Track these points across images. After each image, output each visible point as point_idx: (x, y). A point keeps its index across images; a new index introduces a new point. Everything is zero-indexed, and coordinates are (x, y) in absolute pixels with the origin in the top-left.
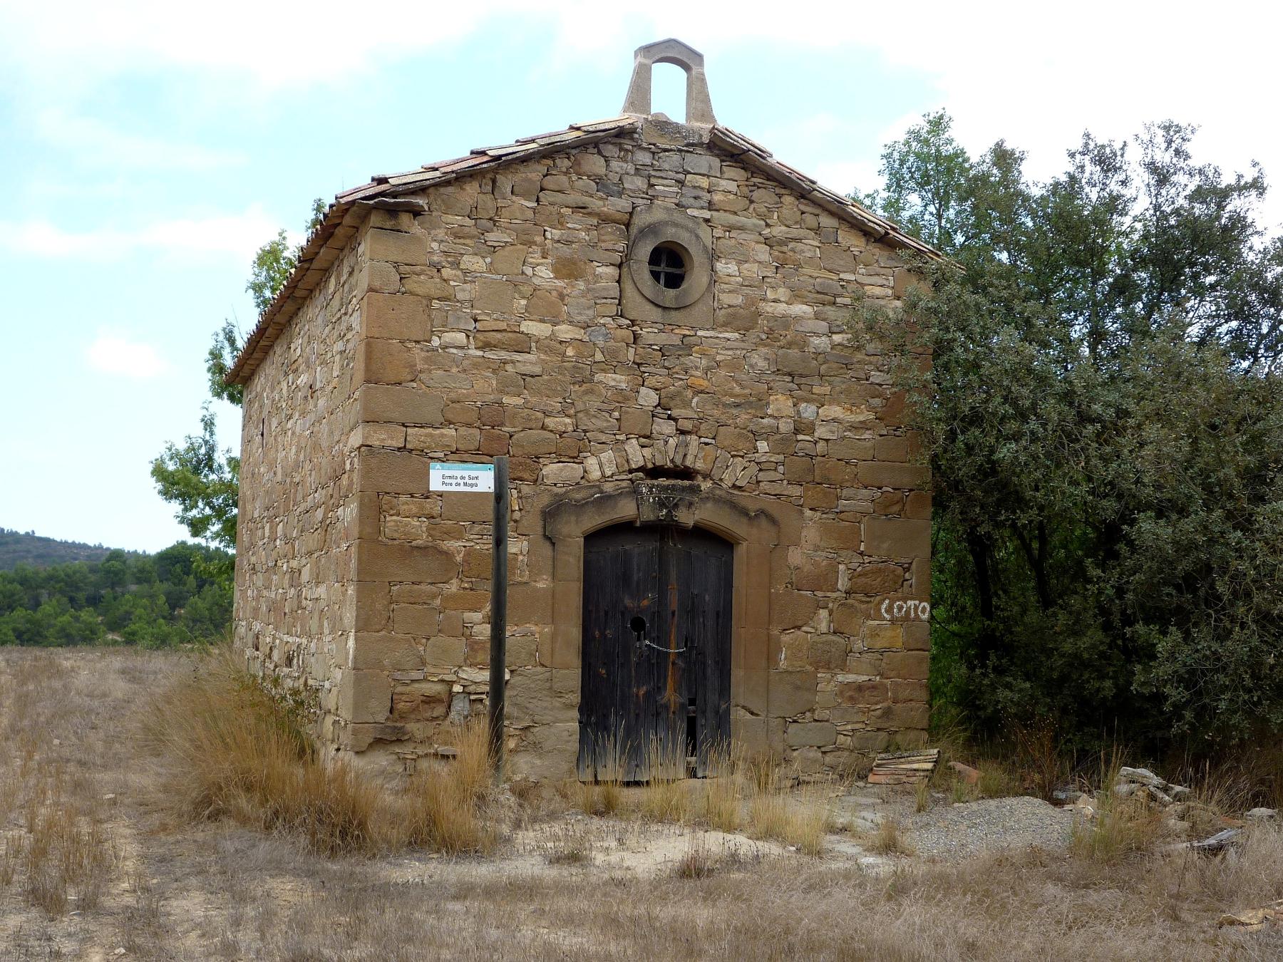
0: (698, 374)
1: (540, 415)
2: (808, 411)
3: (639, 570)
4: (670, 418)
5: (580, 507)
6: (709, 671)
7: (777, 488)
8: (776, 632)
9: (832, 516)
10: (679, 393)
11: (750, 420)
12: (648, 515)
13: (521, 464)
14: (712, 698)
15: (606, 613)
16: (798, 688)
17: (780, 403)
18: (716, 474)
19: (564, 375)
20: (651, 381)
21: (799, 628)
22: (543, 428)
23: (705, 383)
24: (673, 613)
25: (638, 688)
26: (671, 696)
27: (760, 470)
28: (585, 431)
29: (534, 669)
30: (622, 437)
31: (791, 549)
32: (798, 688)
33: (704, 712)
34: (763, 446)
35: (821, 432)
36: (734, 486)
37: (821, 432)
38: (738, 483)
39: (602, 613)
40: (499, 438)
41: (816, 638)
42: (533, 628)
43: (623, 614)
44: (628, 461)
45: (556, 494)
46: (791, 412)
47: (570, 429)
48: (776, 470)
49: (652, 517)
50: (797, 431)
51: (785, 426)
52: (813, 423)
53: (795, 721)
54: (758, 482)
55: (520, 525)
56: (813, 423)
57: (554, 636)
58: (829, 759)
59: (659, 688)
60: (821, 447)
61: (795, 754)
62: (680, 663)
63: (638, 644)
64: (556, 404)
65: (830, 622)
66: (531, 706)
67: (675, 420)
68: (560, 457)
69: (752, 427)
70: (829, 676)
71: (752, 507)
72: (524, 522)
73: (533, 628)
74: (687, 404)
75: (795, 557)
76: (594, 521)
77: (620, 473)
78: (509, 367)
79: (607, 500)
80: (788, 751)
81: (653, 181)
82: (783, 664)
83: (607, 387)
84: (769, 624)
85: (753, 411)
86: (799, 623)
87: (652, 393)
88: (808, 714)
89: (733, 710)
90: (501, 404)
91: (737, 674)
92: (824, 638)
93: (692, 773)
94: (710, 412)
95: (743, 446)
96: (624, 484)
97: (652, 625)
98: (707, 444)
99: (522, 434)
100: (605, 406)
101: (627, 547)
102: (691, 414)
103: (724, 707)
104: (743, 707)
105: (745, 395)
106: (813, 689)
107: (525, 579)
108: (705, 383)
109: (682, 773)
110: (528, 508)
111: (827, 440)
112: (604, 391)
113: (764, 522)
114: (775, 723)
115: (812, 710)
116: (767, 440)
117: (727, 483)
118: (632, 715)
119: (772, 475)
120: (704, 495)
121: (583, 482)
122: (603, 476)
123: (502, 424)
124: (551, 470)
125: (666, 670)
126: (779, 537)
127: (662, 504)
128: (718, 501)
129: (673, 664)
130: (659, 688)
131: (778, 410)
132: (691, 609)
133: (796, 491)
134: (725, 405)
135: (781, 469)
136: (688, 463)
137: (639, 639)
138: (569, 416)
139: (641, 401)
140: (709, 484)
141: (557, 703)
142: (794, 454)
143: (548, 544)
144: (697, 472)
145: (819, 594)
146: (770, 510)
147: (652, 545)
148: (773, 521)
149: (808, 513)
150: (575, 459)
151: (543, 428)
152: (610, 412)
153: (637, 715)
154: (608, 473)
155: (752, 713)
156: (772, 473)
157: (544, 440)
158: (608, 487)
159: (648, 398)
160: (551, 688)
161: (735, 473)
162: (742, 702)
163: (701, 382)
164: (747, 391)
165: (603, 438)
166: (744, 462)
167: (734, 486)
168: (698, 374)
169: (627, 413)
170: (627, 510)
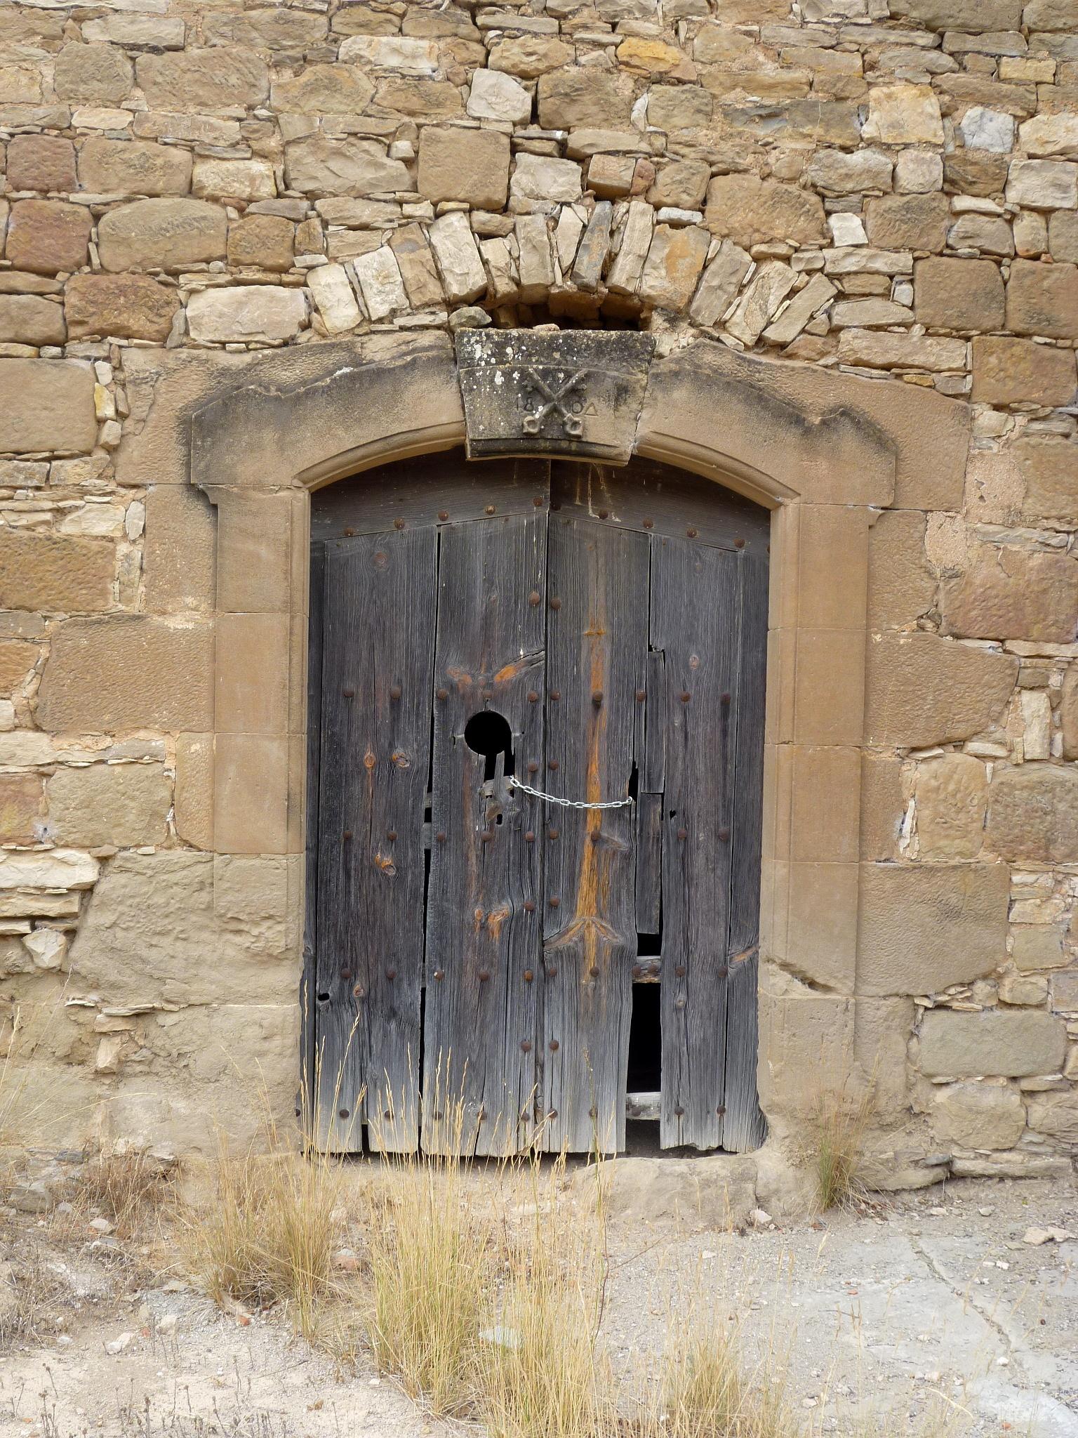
0: (651, 27)
1: (180, 155)
2: (987, 130)
3: (489, 582)
4: (564, 151)
5: (294, 401)
6: (699, 862)
7: (890, 348)
8: (888, 756)
9: (1059, 426)
10: (591, 84)
11: (809, 155)
12: (493, 420)
13: (122, 291)
14: (709, 936)
15: (395, 702)
16: (951, 914)
17: (902, 108)
18: (707, 308)
19: (251, 44)
20: (509, 52)
21: (959, 744)
22: (192, 190)
23: (672, 54)
24: (597, 704)
25: (488, 905)
26: (592, 927)
27: (841, 296)
28: (311, 196)
29: (164, 855)
30: (424, 209)
31: (935, 519)
32: (951, 914)
33: (682, 974)
34: (847, 227)
35: (1027, 187)
36: (761, 342)
37: (1027, 187)
38: (772, 334)
39: (383, 705)
40: (58, 220)
41: (1011, 775)
42: (158, 742)
43: (444, 702)
44: (439, 277)
45: (224, 372)
46: (935, 130)
47: (267, 188)
48: (887, 295)
49: (502, 429)
50: (951, 186)
51: (918, 172)
52: (1001, 165)
53: (940, 1007)
54: (835, 331)
55: (122, 458)
56: (1001, 165)
57: (217, 763)
58: (1040, 1111)
59: (553, 906)
60: (1026, 231)
61: (941, 1096)
62: (618, 840)
63: (488, 788)
64: (223, 125)
65: (1054, 727)
66: (153, 954)
67: (582, 159)
68: (237, 269)
69: (814, 174)
70: (1047, 880)
71: (816, 397)
72: (133, 451)
73: (158, 742)
74: (620, 114)
75: (947, 543)
76: (334, 442)
77: (415, 309)
78: (91, 30)
79: (364, 383)
80: (921, 1088)
81: (874, 54)
82: (908, 847)
83: (378, 74)
84: (866, 729)
85: (818, 131)
86: (960, 731)
87: (512, 86)
88: (981, 988)
89: (763, 968)
90: (65, 129)
91: (774, 873)
92: (1034, 773)
93: (642, 1136)
94: (685, 135)
95: (787, 227)
96: (427, 338)
97: (528, 737)
98: (676, 225)
99: (126, 209)
100: (371, 126)
101: (456, 521)
102: (626, 140)
103: (740, 959)
104: (785, 966)
105: (794, 87)
106: (1000, 914)
107: (136, 608)
108: (672, 54)
109: (611, 1136)
110: (140, 410)
111: (1046, 213)
112: (367, 85)
113: (849, 441)
114: (877, 1011)
115: (994, 977)
116: (861, 210)
117: (742, 330)
118: (470, 980)
119: (876, 311)
120: (663, 367)
121: (303, 337)
122: (366, 319)
123: (69, 185)
124: (214, 308)
125: (574, 854)
126: (896, 487)
127: (532, 393)
128: (706, 381)
129: (596, 839)
130: (553, 906)
131: (894, 125)
132: (648, 694)
133: (951, 354)
134: (730, 114)
135: (904, 292)
136: (619, 277)
137: (490, 775)
138: (264, 156)
139: (477, 107)
140: (686, 336)
141: (232, 946)
142: (948, 251)
143: (199, 508)
144: (649, 304)
145: (1020, 648)
146: (866, 405)
147: (526, 514)
148: (878, 438)
149: (987, 418)
150: (279, 273)
151: (192, 190)
152: (385, 140)
153: (485, 979)
154: (379, 309)
155: (812, 984)
156: (876, 303)
157: (187, 223)
158: (379, 349)
159: (499, 99)
160: (209, 907)
161: (765, 305)
162: (781, 954)
163: (659, 49)
164: (800, 75)
165: (365, 211)
166: (792, 275)
167: (761, 342)
168: (651, 27)
169: (434, 140)
170: (432, 411)
